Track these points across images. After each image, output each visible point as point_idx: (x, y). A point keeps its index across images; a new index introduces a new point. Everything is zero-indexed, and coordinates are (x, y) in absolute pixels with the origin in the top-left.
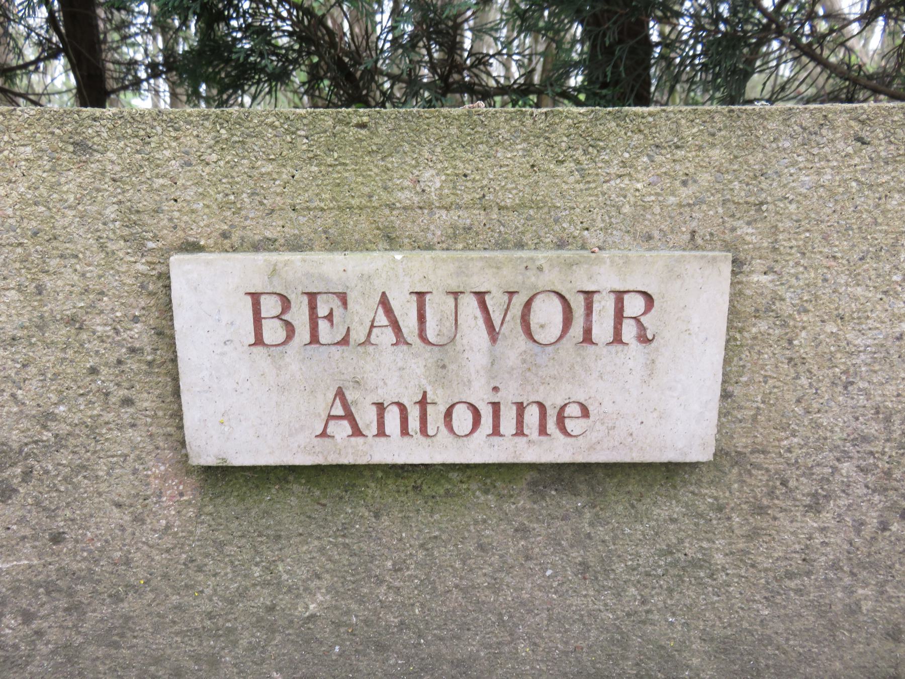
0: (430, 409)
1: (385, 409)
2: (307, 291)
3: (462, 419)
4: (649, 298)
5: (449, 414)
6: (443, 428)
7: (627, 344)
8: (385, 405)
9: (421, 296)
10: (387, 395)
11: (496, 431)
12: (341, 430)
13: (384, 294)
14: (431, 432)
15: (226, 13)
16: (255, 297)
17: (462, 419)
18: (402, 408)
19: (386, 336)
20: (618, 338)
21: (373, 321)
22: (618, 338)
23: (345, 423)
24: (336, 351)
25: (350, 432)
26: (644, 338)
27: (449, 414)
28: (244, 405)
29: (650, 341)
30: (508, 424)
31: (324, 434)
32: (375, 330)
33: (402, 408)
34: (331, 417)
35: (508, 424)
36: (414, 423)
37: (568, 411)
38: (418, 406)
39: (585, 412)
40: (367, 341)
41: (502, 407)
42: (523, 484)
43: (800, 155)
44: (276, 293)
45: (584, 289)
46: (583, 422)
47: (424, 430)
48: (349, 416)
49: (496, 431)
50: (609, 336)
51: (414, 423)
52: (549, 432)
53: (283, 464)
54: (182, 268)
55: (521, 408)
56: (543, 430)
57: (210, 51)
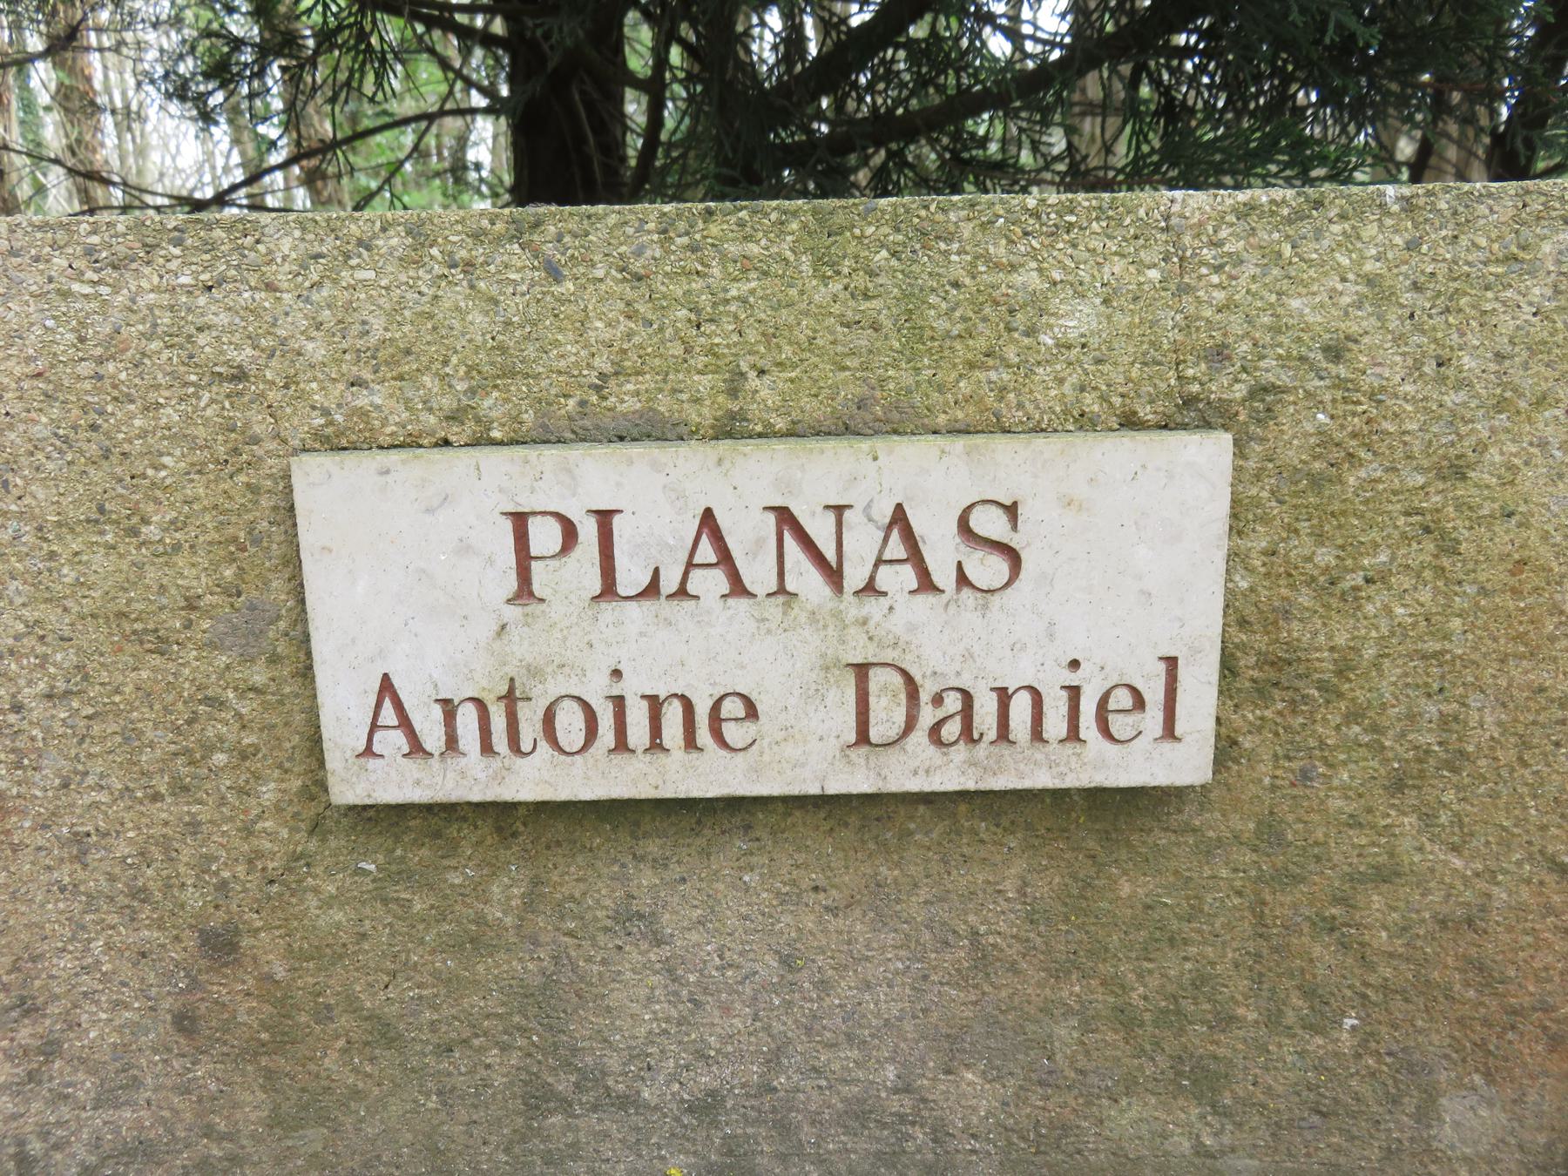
0: (523, 711)
3: (570, 724)
4: (1012, 510)
7: (697, 597)
8: (662, 698)
10: (456, 690)
12: (392, 741)
14: (526, 746)
15: (1201, 46)
16: (520, 521)
17: (570, 724)
19: (709, 583)
30: (638, 732)
31: (368, 751)
37: (1112, 705)
38: (502, 705)
39: (752, 712)
40: (682, 592)
41: (628, 702)
43: (1356, 259)
46: (750, 729)
49: (621, 744)
52: (699, 743)
53: (498, 799)
54: (328, 492)
56: (690, 742)
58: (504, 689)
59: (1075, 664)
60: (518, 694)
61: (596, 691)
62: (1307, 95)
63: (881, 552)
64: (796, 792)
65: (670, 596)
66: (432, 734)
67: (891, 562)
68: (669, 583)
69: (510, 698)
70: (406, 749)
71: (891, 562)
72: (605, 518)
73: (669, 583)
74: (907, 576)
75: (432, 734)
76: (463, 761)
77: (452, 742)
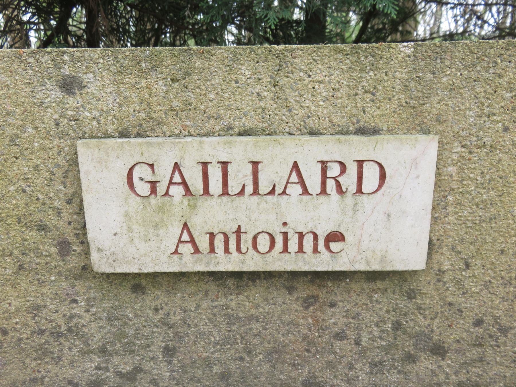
0: (243, 237)
1: (304, 236)
2: (202, 161)
3: (263, 243)
5: (255, 239)
6: (251, 248)
9: (255, 164)
11: (285, 250)
12: (187, 249)
13: (295, 163)
14: (244, 250)
16: (324, 163)
17: (263, 243)
18: (226, 236)
19: (295, 190)
20: (324, 191)
21: (172, 178)
22: (324, 191)
23: (190, 246)
24: (270, 198)
25: (192, 251)
26: (339, 186)
27: (255, 239)
28: (122, 233)
29: (344, 192)
30: (293, 245)
31: (176, 252)
32: (180, 245)
33: (226, 236)
34: (180, 241)
35: (293, 245)
36: (233, 246)
38: (235, 235)
40: (284, 192)
42: (129, 286)
44: (146, 163)
45: (220, 161)
47: (239, 249)
48: (192, 241)
49: (285, 250)
50: (318, 189)
51: (233, 246)
54: (88, 154)
55: (301, 235)
56: (315, 250)
57: (293, 26)
58: (235, 230)
59: (285, 224)
60: (242, 230)
61: (277, 230)
62: (216, 25)
63: (172, 178)
64: (330, 269)
65: (279, 195)
66: (204, 244)
67: (290, 183)
68: (279, 190)
69: (238, 232)
70: (192, 251)
71: (290, 183)
72: (224, 164)
73: (279, 190)
74: (298, 189)
75: (204, 244)
76: (305, 256)
77: (212, 250)
